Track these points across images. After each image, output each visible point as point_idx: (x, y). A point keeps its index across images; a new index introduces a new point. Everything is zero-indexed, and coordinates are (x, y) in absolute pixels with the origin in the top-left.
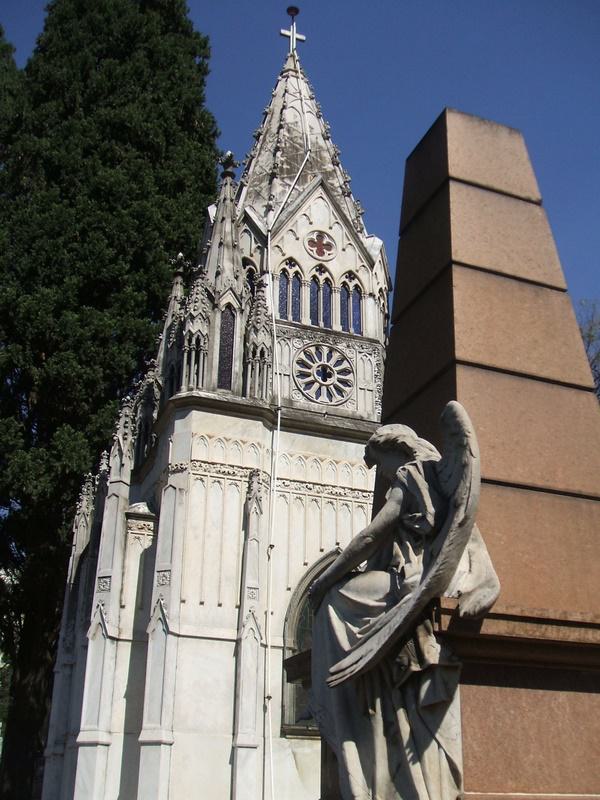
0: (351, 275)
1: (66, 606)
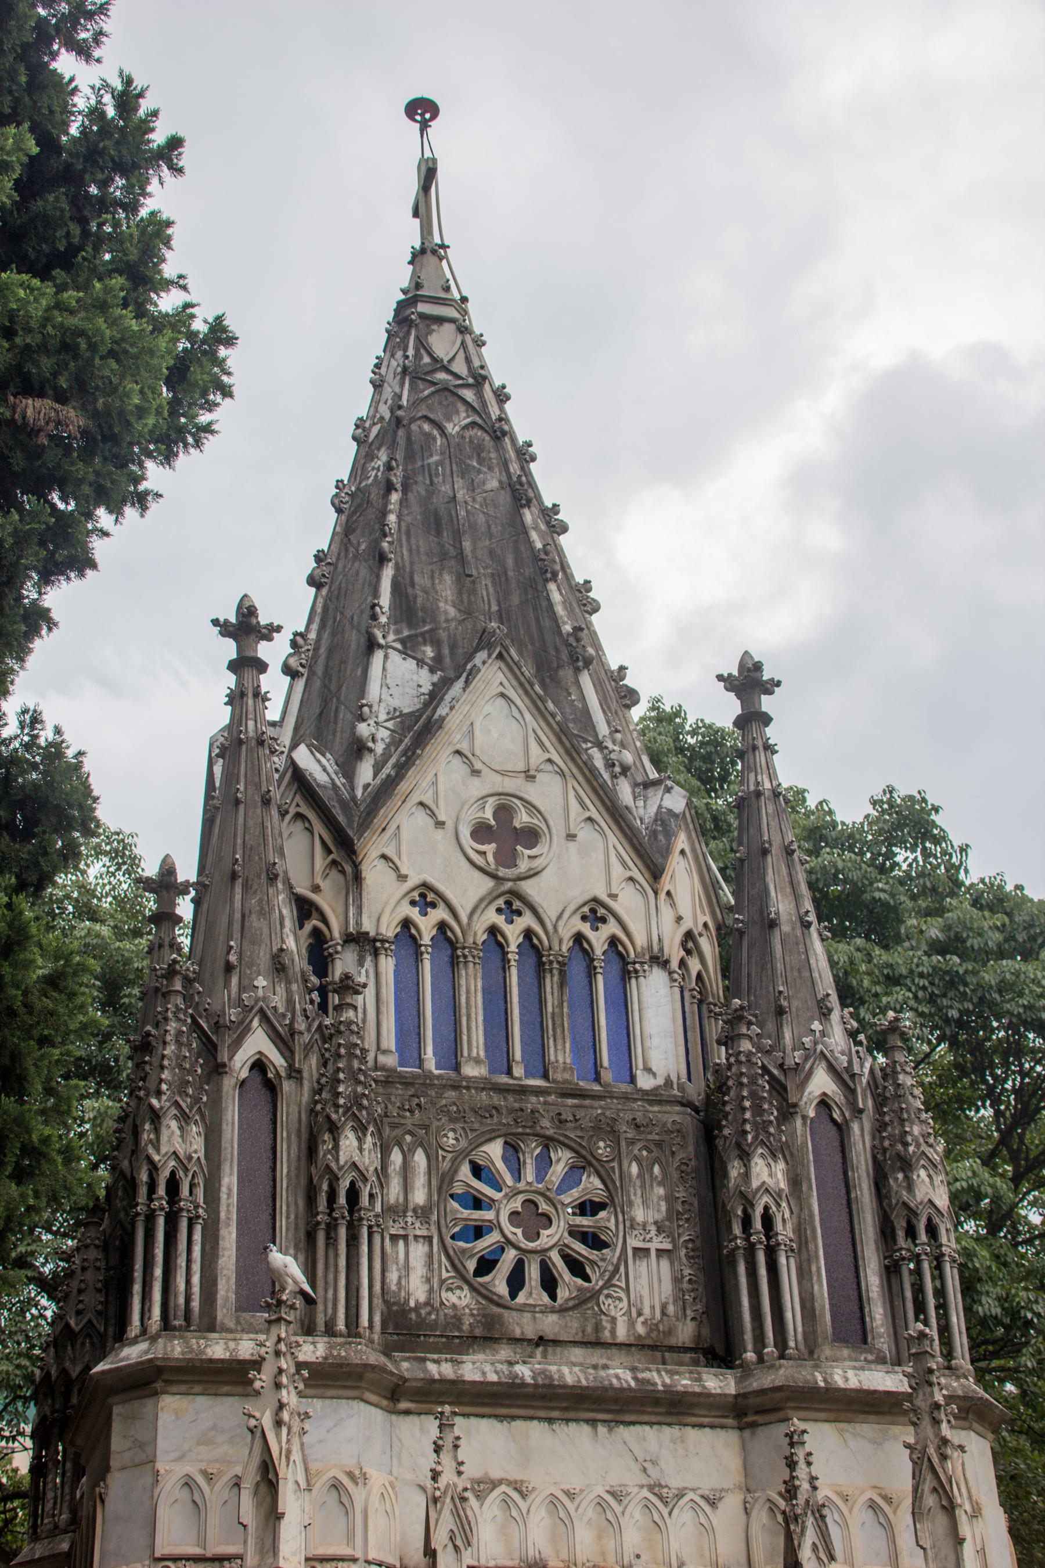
1: (243, 765)
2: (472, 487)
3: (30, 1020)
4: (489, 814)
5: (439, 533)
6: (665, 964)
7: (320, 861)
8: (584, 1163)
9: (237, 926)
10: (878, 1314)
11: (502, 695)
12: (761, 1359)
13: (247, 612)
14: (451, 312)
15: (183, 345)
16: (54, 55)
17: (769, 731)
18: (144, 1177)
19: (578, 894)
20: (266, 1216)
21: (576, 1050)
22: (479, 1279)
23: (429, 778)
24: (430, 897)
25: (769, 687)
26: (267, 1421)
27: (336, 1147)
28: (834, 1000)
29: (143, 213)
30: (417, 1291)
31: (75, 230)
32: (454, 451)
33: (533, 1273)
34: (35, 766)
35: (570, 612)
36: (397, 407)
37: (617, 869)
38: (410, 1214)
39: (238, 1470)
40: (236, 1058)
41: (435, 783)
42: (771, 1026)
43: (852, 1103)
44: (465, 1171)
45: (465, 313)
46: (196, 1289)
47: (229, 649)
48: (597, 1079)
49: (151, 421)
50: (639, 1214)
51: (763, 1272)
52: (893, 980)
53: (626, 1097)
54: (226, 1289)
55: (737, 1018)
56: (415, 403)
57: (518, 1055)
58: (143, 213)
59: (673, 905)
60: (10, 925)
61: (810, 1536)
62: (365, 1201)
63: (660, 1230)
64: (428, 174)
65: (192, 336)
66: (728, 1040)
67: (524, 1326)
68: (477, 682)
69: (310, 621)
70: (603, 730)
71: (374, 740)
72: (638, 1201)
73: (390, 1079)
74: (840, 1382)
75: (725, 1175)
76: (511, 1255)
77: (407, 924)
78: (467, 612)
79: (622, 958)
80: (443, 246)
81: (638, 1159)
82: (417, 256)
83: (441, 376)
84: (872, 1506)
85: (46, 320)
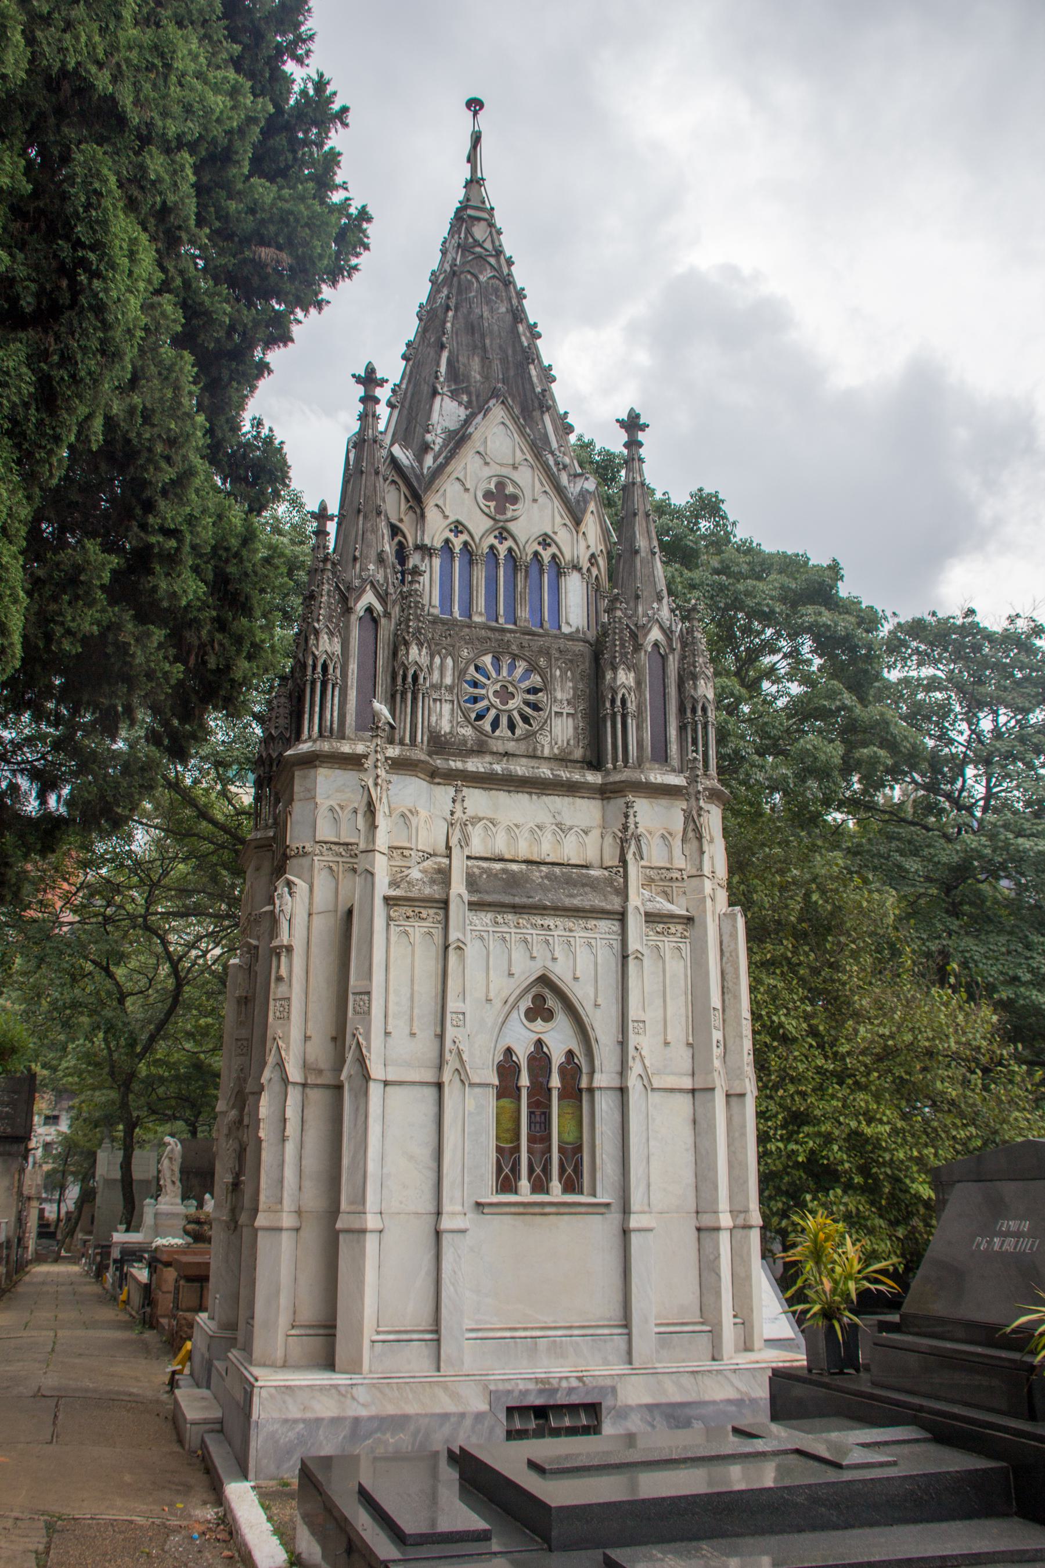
0: (546, 541)
2: (492, 311)
3: (255, 579)
4: (492, 486)
5: (473, 334)
6: (579, 570)
7: (403, 506)
8: (533, 668)
9: (360, 538)
10: (674, 749)
12: (615, 768)
13: (370, 370)
14: (485, 215)
15: (344, 221)
16: (284, 63)
17: (641, 451)
18: (310, 662)
19: (537, 531)
20: (371, 685)
21: (532, 611)
23: (462, 465)
25: (643, 427)
26: (370, 783)
27: (408, 653)
28: (665, 593)
29: (326, 148)
30: (445, 727)
31: (290, 156)
32: (483, 290)
33: (504, 721)
34: (258, 448)
35: (541, 381)
36: (453, 265)
37: (558, 519)
39: (356, 805)
41: (465, 468)
42: (632, 604)
43: (670, 645)
44: (472, 668)
45: (492, 216)
46: (336, 719)
47: (360, 391)
48: (542, 626)
49: (326, 262)
50: (559, 695)
51: (619, 726)
52: (693, 587)
53: (556, 637)
54: (351, 719)
55: (615, 600)
56: (463, 264)
57: (502, 612)
58: (326, 148)
59: (586, 540)
60: (247, 530)
61: (633, 848)
62: (421, 680)
63: (569, 703)
64: (476, 139)
65: (349, 216)
66: (609, 611)
67: (498, 746)
68: (490, 415)
69: (403, 378)
70: (554, 445)
72: (559, 689)
73: (436, 621)
74: (652, 779)
75: (604, 677)
76: (493, 712)
77: (447, 541)
78: (486, 378)
79: (558, 565)
80: (483, 179)
81: (560, 668)
82: (468, 184)
83: (478, 250)
84: (663, 837)
85: (273, 204)
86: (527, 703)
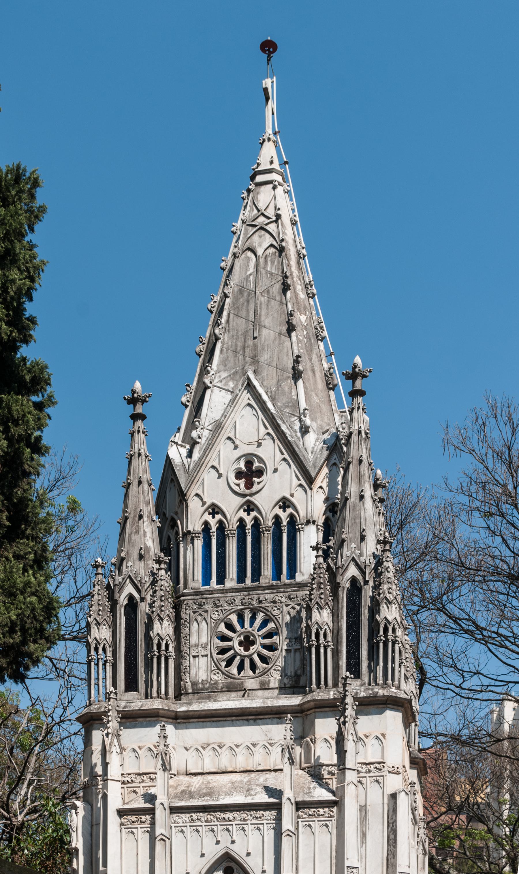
11: (249, 405)
22: (226, 669)
23: (216, 452)
24: (216, 510)
37: (295, 482)
38: (200, 647)
40: (121, 597)
51: (163, 665)
71: (199, 438)
86: (265, 647)
